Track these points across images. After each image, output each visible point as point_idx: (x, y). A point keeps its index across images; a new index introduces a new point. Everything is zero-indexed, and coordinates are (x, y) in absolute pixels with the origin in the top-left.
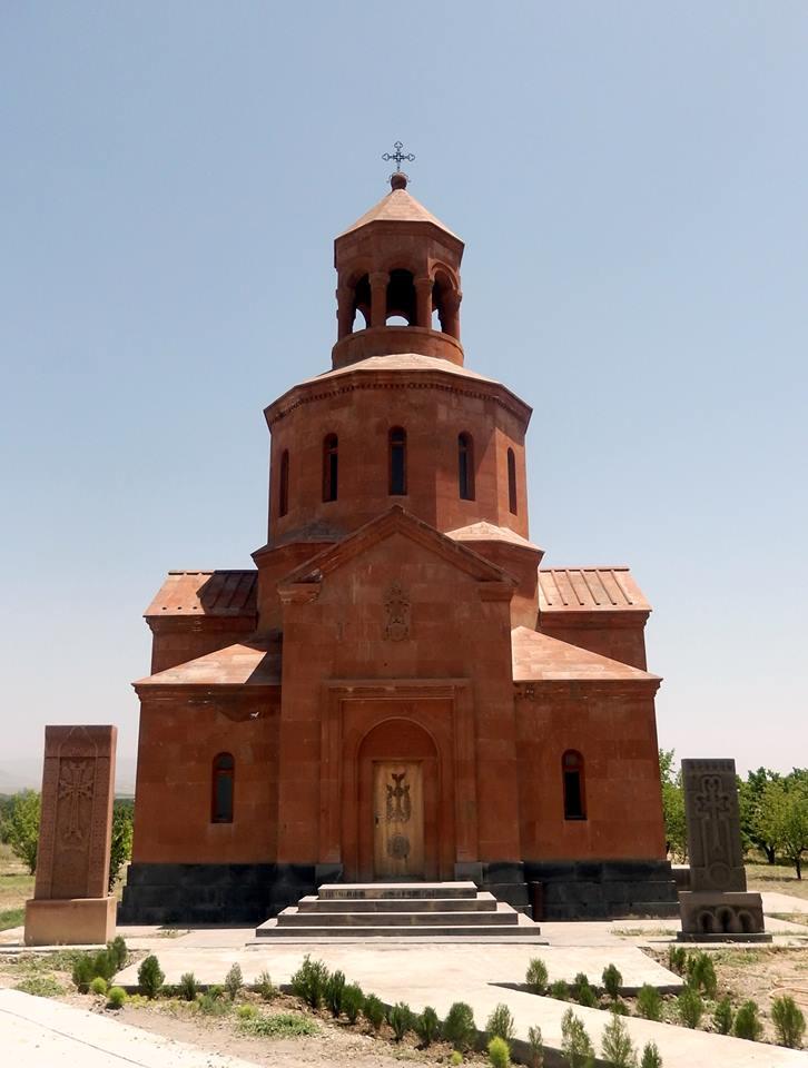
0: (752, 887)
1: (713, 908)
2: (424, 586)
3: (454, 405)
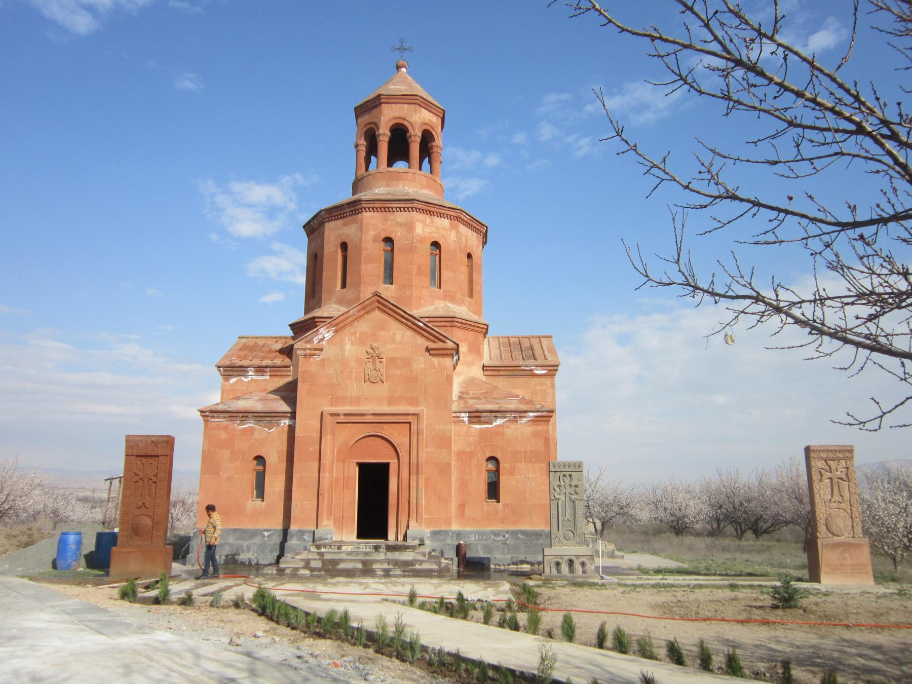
0: (835, 570)
1: (561, 557)
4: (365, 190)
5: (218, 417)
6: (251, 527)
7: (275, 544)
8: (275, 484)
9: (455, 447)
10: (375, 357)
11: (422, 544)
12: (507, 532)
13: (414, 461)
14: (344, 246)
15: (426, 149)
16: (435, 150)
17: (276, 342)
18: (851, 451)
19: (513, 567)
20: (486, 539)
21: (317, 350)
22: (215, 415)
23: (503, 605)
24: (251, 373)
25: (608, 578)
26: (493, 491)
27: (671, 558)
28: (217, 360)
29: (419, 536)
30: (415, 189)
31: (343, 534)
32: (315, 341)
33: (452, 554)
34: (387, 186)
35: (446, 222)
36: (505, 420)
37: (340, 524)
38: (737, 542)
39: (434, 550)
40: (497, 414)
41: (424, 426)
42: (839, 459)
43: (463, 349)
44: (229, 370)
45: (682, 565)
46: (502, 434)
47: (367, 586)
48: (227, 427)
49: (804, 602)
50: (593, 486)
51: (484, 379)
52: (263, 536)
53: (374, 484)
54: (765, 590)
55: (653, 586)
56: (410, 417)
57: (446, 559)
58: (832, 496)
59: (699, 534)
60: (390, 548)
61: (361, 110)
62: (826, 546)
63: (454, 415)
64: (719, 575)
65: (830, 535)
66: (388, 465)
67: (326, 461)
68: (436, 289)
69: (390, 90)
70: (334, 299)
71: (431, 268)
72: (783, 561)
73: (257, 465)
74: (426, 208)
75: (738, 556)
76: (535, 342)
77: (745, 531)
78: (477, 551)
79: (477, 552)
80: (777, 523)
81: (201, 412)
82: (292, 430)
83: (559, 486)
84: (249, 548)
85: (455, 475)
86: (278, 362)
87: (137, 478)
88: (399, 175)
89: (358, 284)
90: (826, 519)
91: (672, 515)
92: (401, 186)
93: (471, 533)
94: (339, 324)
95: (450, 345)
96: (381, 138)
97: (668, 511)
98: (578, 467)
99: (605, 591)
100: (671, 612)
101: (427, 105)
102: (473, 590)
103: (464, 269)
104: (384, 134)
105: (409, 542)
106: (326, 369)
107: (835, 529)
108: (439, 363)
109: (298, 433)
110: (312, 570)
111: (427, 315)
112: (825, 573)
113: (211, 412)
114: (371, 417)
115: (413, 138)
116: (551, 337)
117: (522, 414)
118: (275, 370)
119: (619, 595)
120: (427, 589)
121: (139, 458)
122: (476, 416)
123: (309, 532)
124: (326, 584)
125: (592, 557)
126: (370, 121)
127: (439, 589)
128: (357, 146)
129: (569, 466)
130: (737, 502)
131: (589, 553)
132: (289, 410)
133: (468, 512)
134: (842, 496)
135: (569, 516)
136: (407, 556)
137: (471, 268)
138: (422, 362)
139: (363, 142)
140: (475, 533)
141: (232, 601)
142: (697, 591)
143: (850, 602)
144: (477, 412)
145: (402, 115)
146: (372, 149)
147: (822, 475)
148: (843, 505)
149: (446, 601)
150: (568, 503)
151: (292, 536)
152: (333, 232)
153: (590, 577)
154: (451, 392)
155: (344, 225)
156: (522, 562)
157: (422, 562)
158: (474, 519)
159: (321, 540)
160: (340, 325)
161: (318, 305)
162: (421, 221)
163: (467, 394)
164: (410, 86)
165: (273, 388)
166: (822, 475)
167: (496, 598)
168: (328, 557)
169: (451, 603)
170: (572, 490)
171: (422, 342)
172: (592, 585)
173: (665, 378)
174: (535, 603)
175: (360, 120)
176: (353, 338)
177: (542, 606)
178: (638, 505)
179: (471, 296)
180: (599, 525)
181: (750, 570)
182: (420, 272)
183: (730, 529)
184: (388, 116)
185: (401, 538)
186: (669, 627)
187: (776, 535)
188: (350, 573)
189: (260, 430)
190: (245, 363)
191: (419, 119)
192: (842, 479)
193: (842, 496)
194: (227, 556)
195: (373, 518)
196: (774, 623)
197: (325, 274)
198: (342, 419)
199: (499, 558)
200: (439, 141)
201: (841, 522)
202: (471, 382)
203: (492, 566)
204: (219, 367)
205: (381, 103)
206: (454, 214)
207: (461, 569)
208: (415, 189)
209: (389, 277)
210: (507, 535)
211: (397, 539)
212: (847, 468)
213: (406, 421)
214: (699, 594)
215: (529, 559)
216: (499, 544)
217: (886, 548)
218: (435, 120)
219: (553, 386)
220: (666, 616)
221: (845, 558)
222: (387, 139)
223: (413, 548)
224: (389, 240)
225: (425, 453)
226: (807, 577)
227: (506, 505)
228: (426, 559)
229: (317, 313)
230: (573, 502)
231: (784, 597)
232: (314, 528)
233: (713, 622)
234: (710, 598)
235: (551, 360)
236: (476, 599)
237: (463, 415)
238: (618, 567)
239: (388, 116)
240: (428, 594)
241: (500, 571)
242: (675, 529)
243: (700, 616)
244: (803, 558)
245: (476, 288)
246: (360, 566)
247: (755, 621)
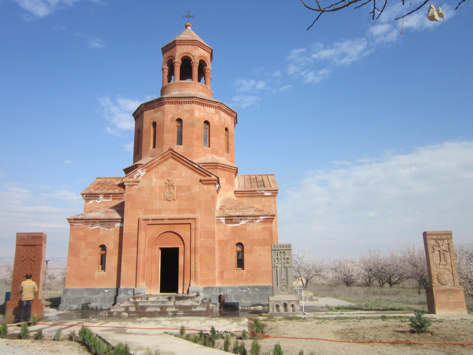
0: (443, 306)
1: (280, 302)
2: (181, 179)
3: (202, 110)
4: (167, 93)
5: (79, 223)
6: (97, 287)
7: (112, 297)
8: (112, 261)
9: (217, 238)
10: (170, 185)
11: (198, 295)
13: (193, 246)
14: (154, 124)
15: (202, 72)
16: (207, 71)
17: (117, 180)
18: (450, 234)
19: (252, 308)
20: (237, 291)
21: (136, 182)
22: (77, 221)
23: (240, 334)
24: (101, 198)
25: (308, 313)
26: (240, 263)
27: (344, 299)
28: (82, 191)
29: (196, 291)
30: (196, 93)
31: (151, 290)
32: (135, 176)
33: (216, 301)
34: (180, 91)
35: (212, 110)
36: (246, 221)
37: (149, 284)
38: (381, 289)
39: (205, 299)
40: (242, 218)
41: (199, 225)
42: (444, 239)
43: (222, 181)
44: (89, 196)
45: (352, 304)
46: (245, 230)
47: (159, 322)
48: (84, 228)
49: (430, 328)
50: (301, 260)
51: (235, 198)
52: (105, 292)
53: (170, 259)
54: (403, 319)
55: (335, 319)
56: (191, 220)
57: (212, 304)
58: (440, 261)
59: (359, 285)
60: (178, 298)
61: (165, 49)
62: (438, 291)
63: (216, 219)
64: (375, 310)
65: (440, 285)
66: (177, 249)
67: (141, 247)
68: (207, 148)
69: (181, 38)
70: (148, 154)
71: (204, 137)
72: (408, 300)
73: (102, 250)
74: (201, 102)
75: (383, 297)
76: (265, 178)
77: (384, 283)
78: (231, 299)
79: (231, 300)
80: (402, 277)
81: (69, 220)
82: (121, 229)
83: (277, 259)
84: (96, 300)
85: (217, 254)
86: (117, 191)
87: (23, 259)
88: (186, 86)
89: (162, 146)
90: (438, 275)
91: (345, 275)
92: (187, 90)
93: (227, 288)
94: (149, 168)
95: (214, 178)
96: (176, 64)
97: (342, 273)
98: (288, 248)
99: (306, 323)
100: (347, 337)
101: (202, 46)
102: (224, 325)
103: (223, 137)
104: (178, 62)
105: (191, 295)
106: (141, 193)
107: (443, 281)
108: (208, 189)
109: (125, 231)
110: (129, 312)
111: (202, 162)
112: (438, 308)
113: (74, 219)
114: (168, 221)
115: (194, 64)
116: (274, 175)
117: (257, 218)
118: (115, 195)
119: (315, 325)
120: (196, 324)
121: (24, 247)
122: (229, 219)
123: (131, 289)
124: (134, 322)
125: (298, 301)
126: (170, 55)
127: (203, 324)
128: (163, 69)
129: (283, 247)
130: (380, 267)
131: (296, 299)
132: (120, 217)
133: (225, 276)
134: (446, 261)
135: (283, 276)
136: (188, 303)
137: (227, 136)
138: (197, 188)
139: (166, 67)
140: (230, 288)
141: (68, 335)
142: (362, 321)
143: (458, 326)
144: (230, 217)
145: (188, 51)
146: (171, 73)
147: (434, 249)
148: (447, 267)
149: (204, 332)
150: (283, 270)
151: (121, 292)
152: (148, 116)
154: (215, 206)
155: (155, 112)
156: (258, 305)
157: (196, 307)
158: (229, 280)
159: (138, 294)
160: (150, 167)
161: (140, 158)
162: (198, 109)
163: (225, 207)
164: (193, 36)
165: (113, 206)
166: (434, 249)
167: (237, 330)
168: (141, 304)
169: (208, 334)
171: (198, 177)
173: (340, 196)
174: (262, 332)
175: (165, 55)
176: (157, 175)
177: (266, 334)
178: (326, 270)
179: (228, 152)
180: (304, 281)
181: (390, 306)
182: (198, 138)
183: (376, 282)
184: (180, 52)
185: (185, 292)
186: (346, 348)
187: (401, 285)
188: (152, 315)
189: (103, 230)
190: (98, 192)
191: (197, 54)
192: (446, 251)
193: (446, 261)
194: (83, 305)
195: (169, 281)
196: (414, 343)
197: (143, 140)
198: (151, 222)
199: (244, 303)
200: (209, 66)
201: (447, 277)
202: (228, 200)
203: (240, 308)
204: (83, 194)
205: (176, 45)
206: (217, 105)
207: (222, 310)
208: (196, 93)
209: (180, 142)
210: (249, 289)
211: (183, 293)
212: (449, 244)
213: (188, 223)
214: (364, 324)
215: (262, 303)
216: (244, 294)
217: (469, 291)
218: (206, 55)
219: (275, 202)
220: (344, 340)
221: (449, 298)
222: (179, 65)
223: (192, 298)
224: (180, 120)
225: (199, 241)
226: (427, 310)
228: (199, 304)
229: (137, 163)
230: (286, 268)
231: (418, 325)
232: (134, 287)
233: (374, 344)
234: (371, 325)
235: (274, 187)
236: (224, 331)
237: (222, 218)
238: (314, 306)
239: (180, 52)
240: (195, 328)
241: (244, 311)
242: (346, 283)
243: (365, 339)
244: (423, 297)
245: (231, 148)
246: (158, 309)
247: (402, 342)
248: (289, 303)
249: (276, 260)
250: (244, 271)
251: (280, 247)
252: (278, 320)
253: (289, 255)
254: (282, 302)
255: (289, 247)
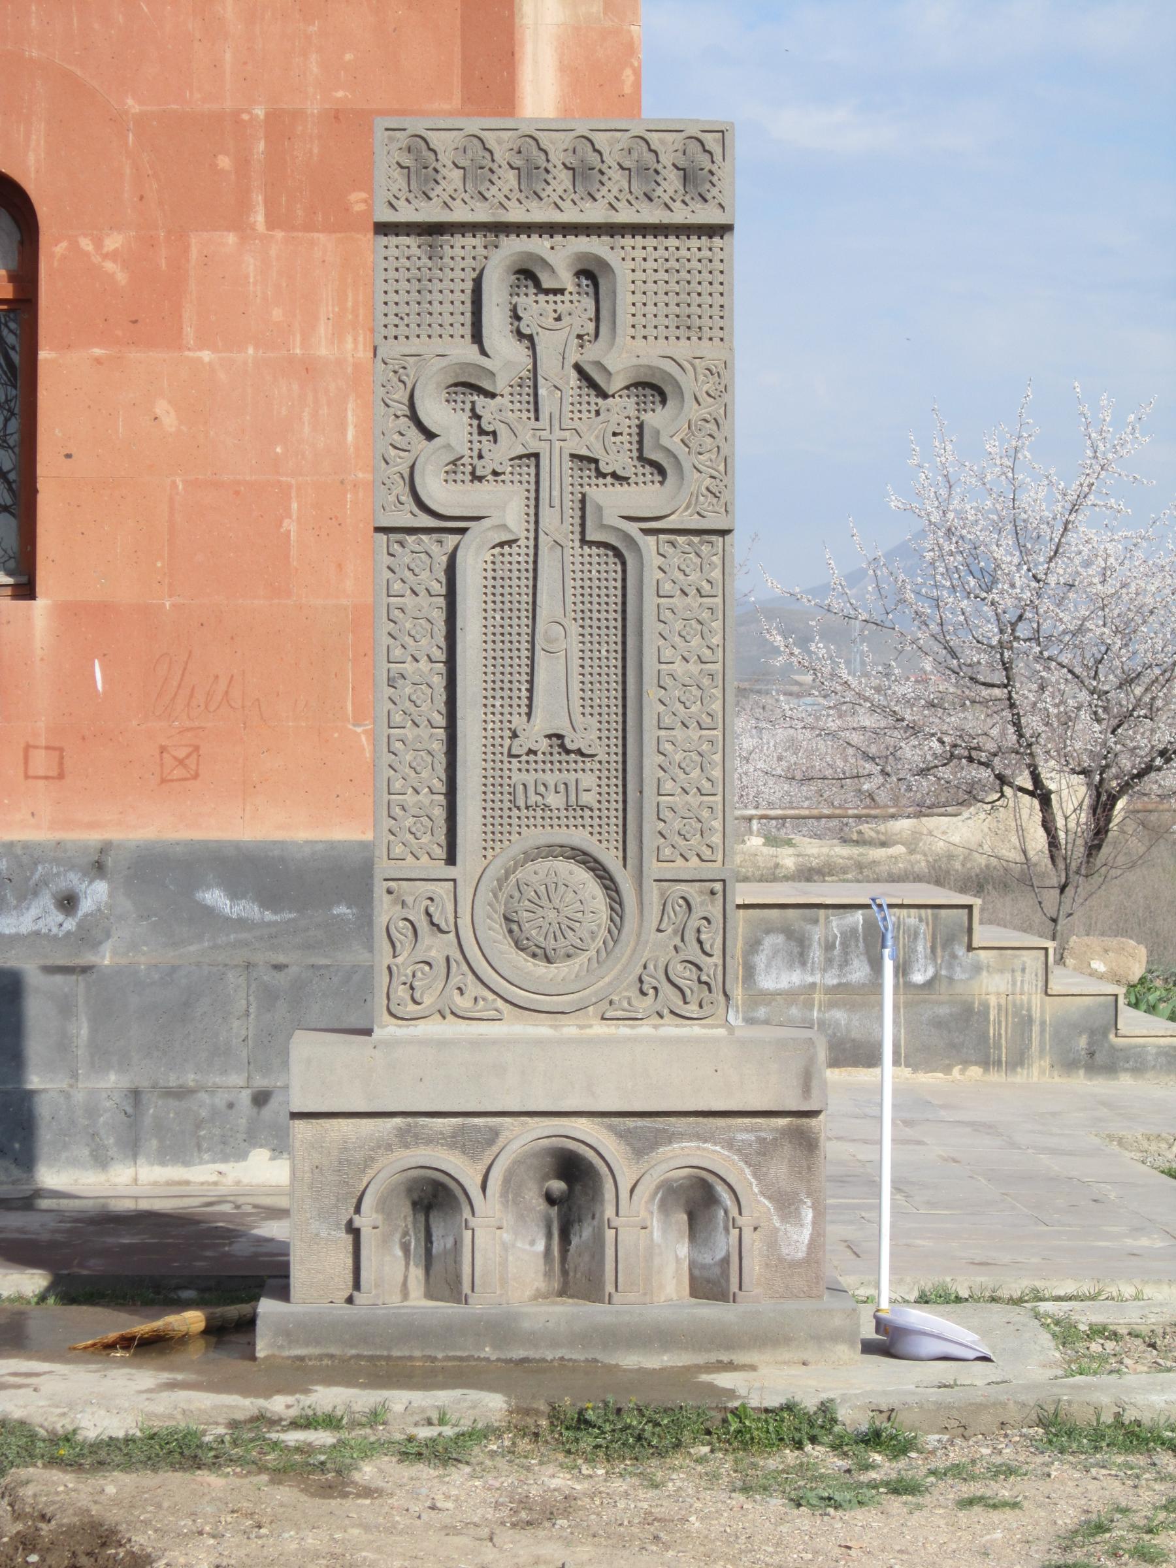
1: (474, 1126)
12: (98, 868)
83: (469, 387)
129: (585, 175)
135: (562, 697)
153: (769, 1338)
170: (604, 430)
172: (747, 1433)
180: (1071, 796)
210: (95, 895)
227: (87, 620)
248: (642, 1146)
249: (434, 411)
250: (40, 606)
251: (531, 172)
252: (413, 1452)
253: (687, 327)
254: (522, 1139)
255: (688, 176)
